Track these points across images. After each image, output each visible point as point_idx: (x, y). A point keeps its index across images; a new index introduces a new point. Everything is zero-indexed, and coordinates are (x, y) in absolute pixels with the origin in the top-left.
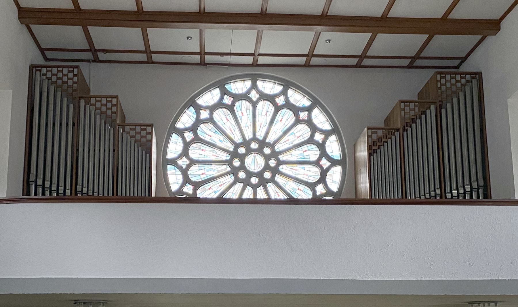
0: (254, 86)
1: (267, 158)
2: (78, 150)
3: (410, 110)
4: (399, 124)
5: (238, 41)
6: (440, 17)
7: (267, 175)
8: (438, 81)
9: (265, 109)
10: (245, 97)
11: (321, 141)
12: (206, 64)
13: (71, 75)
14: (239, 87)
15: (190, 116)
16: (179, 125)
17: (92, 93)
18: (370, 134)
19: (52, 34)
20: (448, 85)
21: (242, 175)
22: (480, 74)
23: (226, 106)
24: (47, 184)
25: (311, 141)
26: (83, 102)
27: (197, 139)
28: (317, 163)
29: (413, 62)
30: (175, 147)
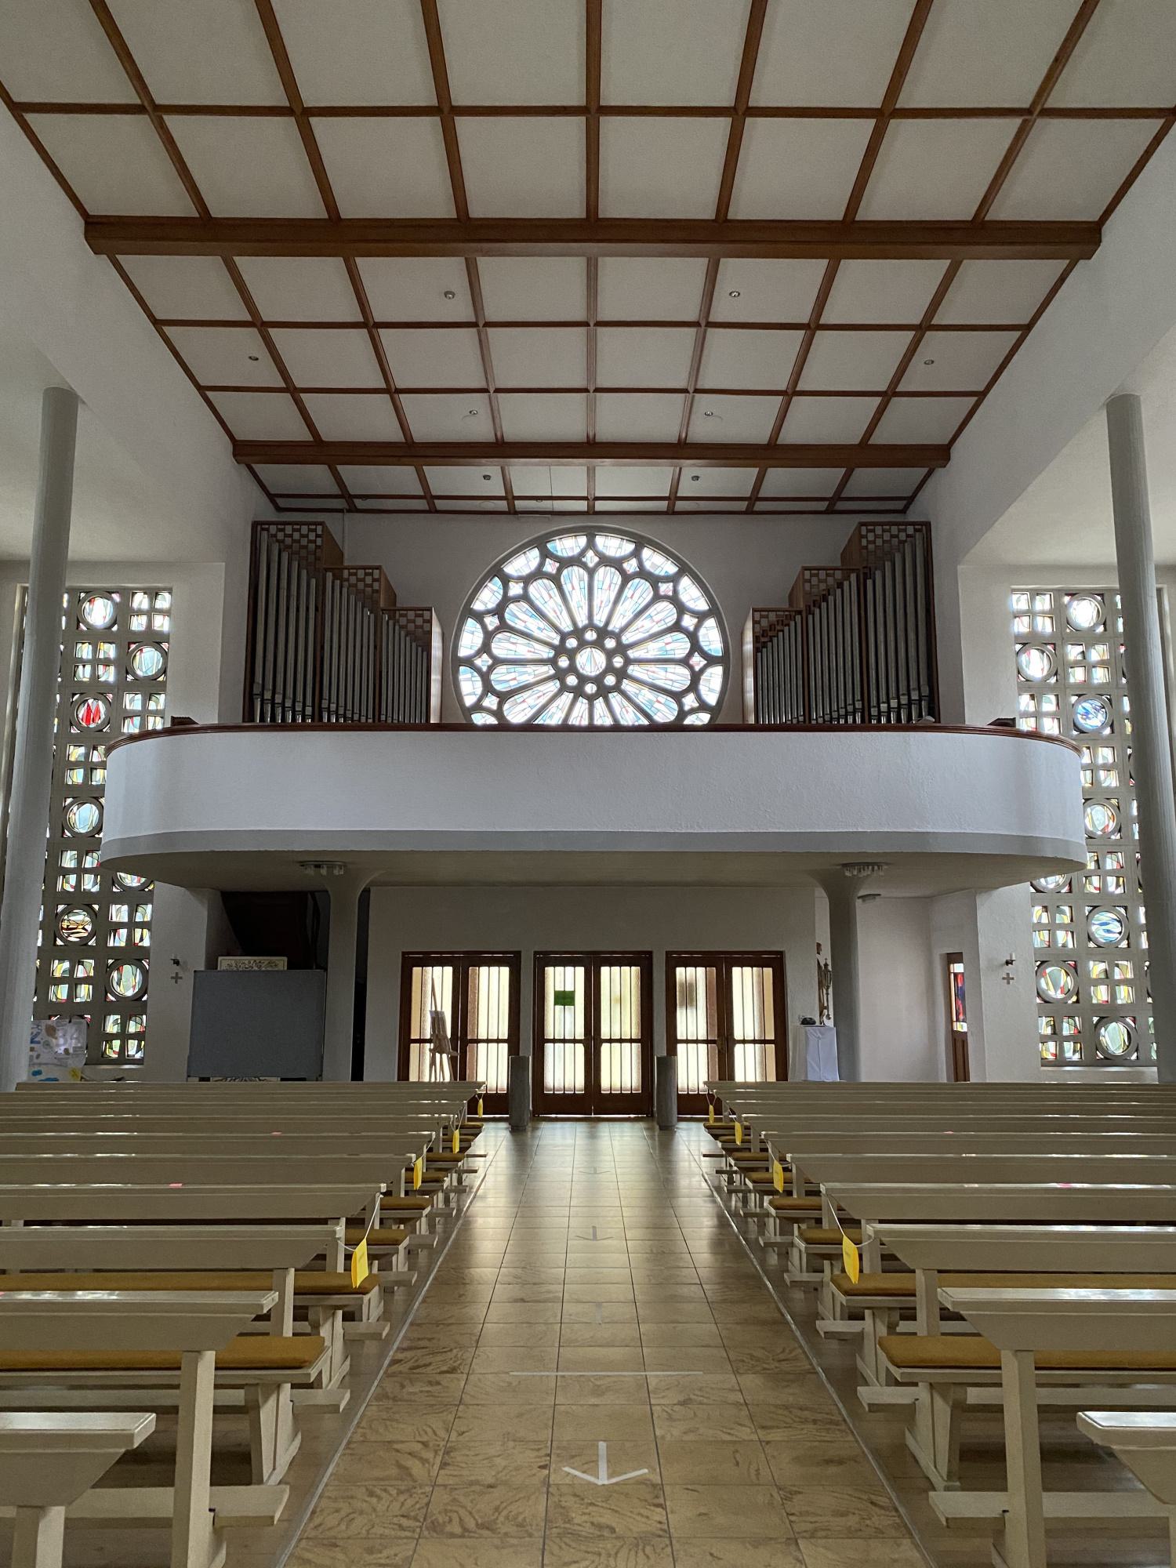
0: (591, 544)
1: (610, 655)
2: (322, 647)
3: (820, 581)
4: (802, 606)
5: (564, 480)
6: (857, 442)
7: (610, 680)
8: (862, 537)
9: (607, 578)
10: (577, 561)
11: (691, 629)
12: (516, 513)
13: (312, 536)
14: (568, 546)
15: (493, 592)
16: (478, 606)
17: (346, 563)
18: (757, 618)
19: (283, 476)
20: (879, 542)
21: (572, 680)
22: (928, 525)
24: (278, 699)
25: (677, 627)
26: (329, 575)
27: (504, 627)
28: (685, 662)
29: (833, 505)
30: (470, 639)
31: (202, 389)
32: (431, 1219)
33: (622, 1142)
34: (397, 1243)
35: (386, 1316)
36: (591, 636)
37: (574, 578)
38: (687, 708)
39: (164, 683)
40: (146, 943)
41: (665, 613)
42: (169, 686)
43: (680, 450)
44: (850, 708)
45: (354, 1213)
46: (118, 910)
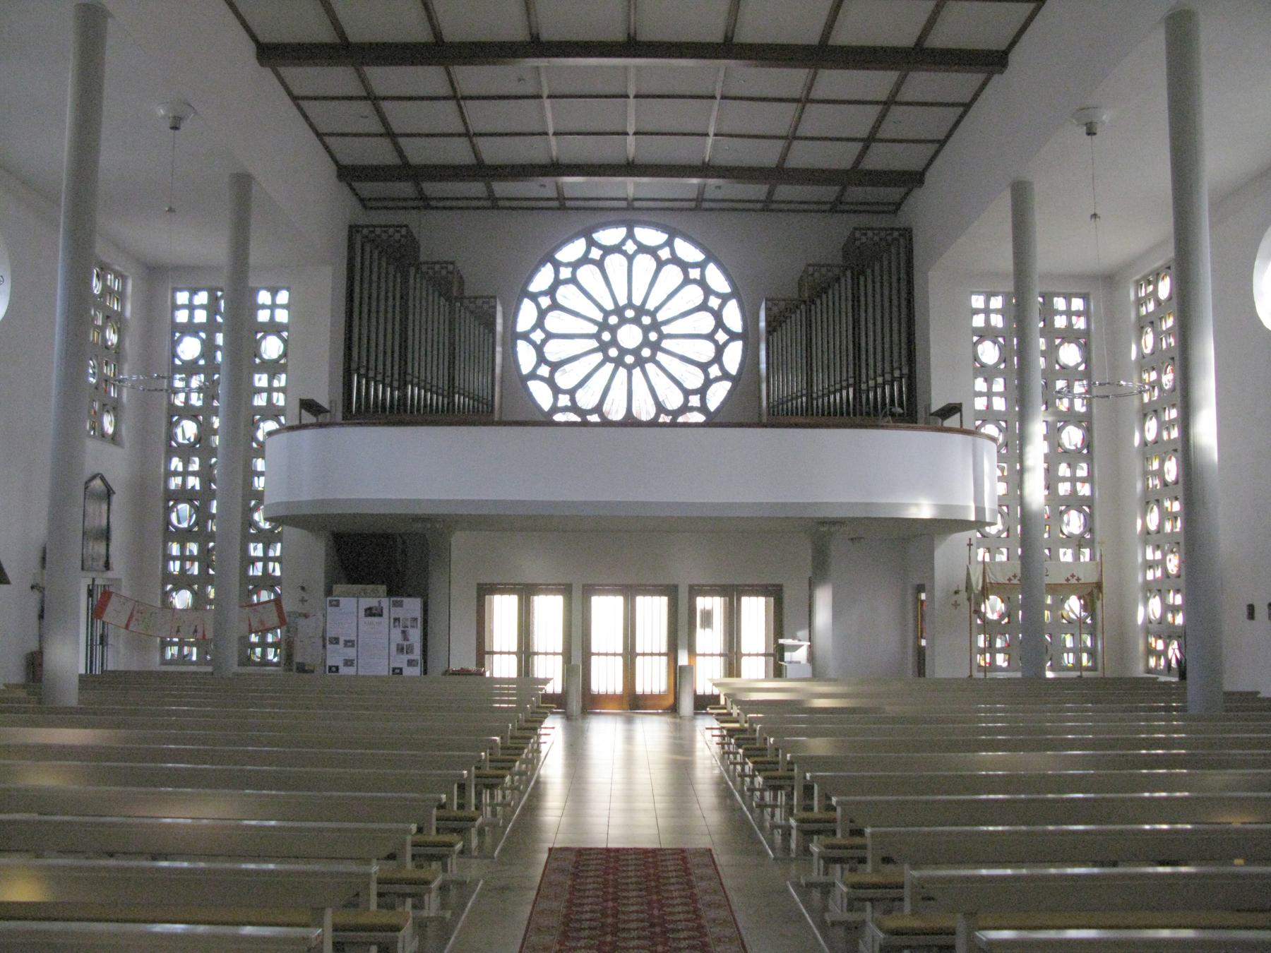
9: (645, 264)
10: (617, 249)
11: (716, 308)
14: (610, 236)
23: (593, 262)
25: (703, 307)
27: (555, 306)
30: (526, 316)
31: (320, 135)
32: (481, 832)
33: (652, 732)
34: (427, 883)
35: (443, 906)
36: (630, 314)
37: (615, 264)
38: (712, 377)
39: (285, 365)
40: (278, 573)
41: (693, 295)
42: (289, 368)
43: (704, 170)
44: (844, 384)
45: (390, 849)
46: (255, 549)
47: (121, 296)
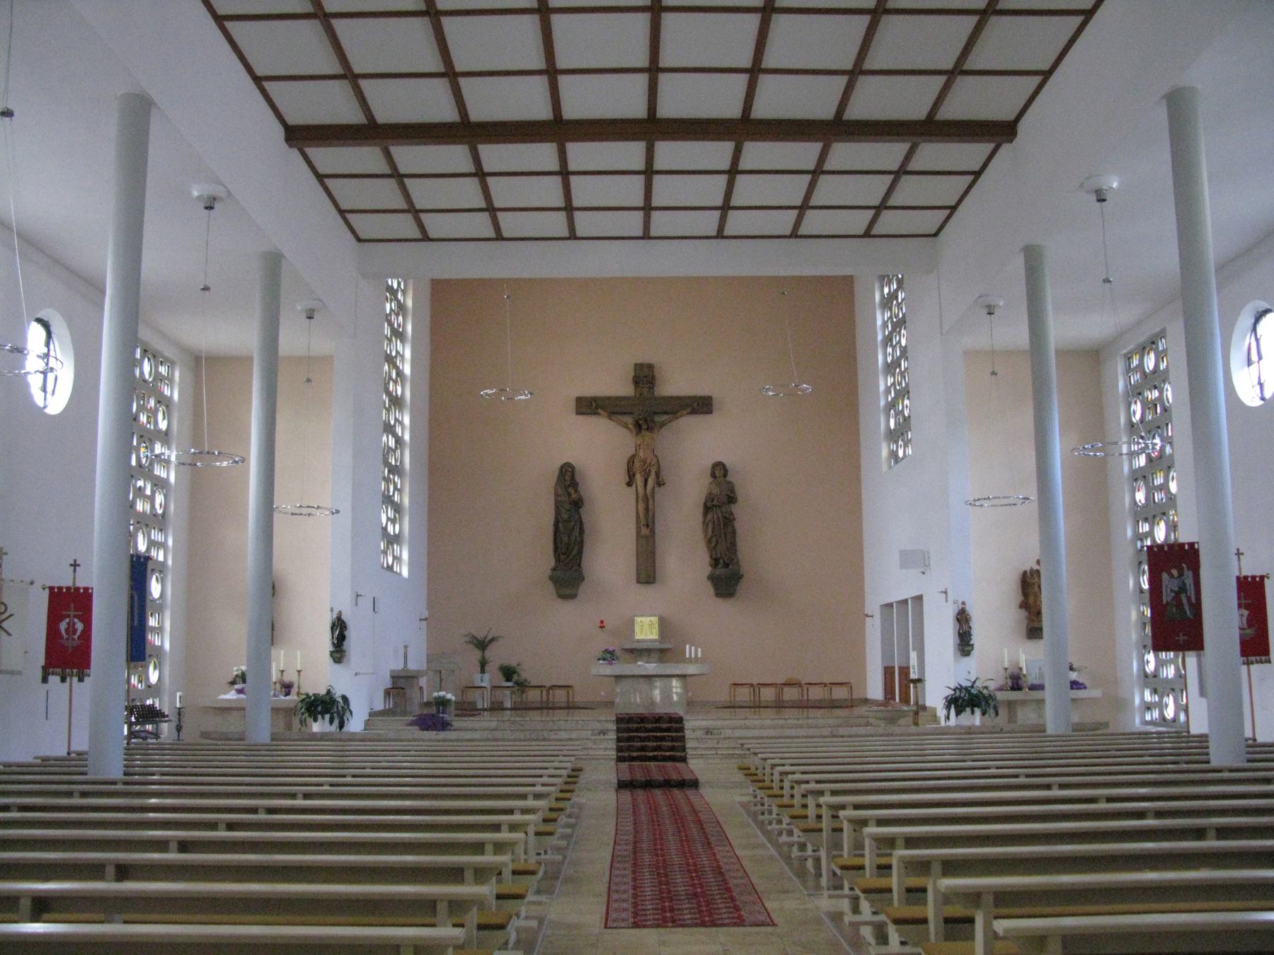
47: (170, 379)
